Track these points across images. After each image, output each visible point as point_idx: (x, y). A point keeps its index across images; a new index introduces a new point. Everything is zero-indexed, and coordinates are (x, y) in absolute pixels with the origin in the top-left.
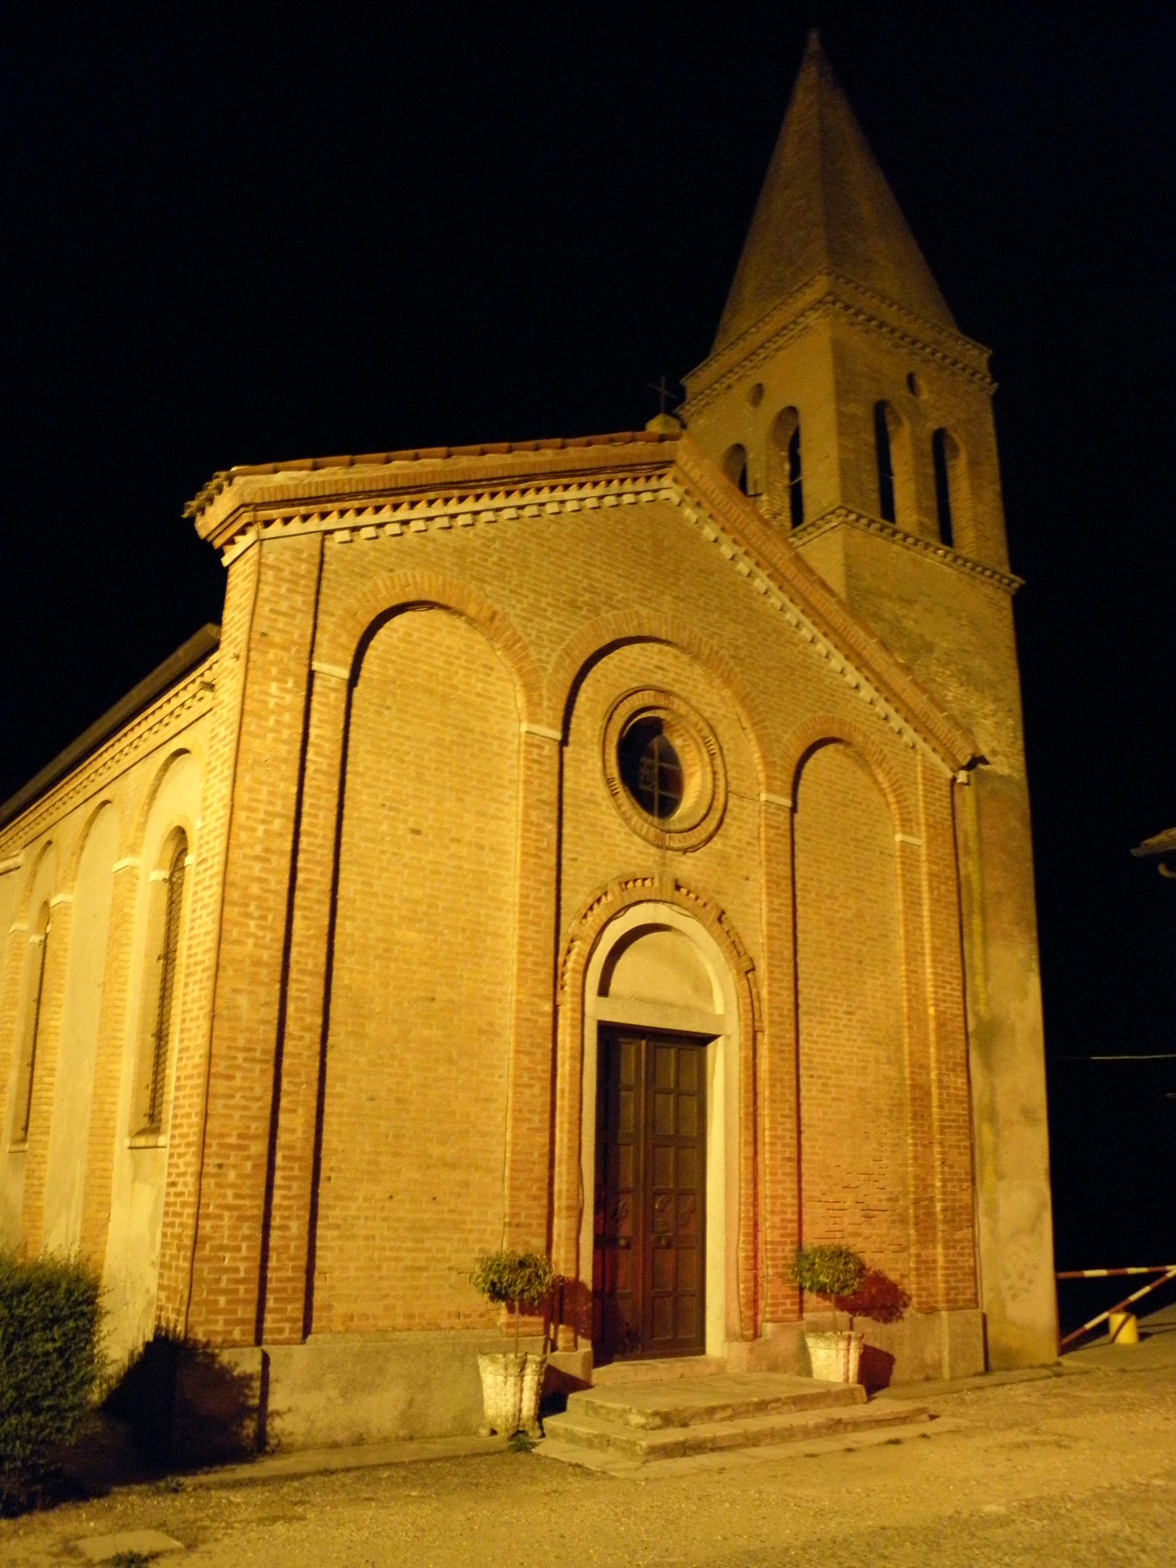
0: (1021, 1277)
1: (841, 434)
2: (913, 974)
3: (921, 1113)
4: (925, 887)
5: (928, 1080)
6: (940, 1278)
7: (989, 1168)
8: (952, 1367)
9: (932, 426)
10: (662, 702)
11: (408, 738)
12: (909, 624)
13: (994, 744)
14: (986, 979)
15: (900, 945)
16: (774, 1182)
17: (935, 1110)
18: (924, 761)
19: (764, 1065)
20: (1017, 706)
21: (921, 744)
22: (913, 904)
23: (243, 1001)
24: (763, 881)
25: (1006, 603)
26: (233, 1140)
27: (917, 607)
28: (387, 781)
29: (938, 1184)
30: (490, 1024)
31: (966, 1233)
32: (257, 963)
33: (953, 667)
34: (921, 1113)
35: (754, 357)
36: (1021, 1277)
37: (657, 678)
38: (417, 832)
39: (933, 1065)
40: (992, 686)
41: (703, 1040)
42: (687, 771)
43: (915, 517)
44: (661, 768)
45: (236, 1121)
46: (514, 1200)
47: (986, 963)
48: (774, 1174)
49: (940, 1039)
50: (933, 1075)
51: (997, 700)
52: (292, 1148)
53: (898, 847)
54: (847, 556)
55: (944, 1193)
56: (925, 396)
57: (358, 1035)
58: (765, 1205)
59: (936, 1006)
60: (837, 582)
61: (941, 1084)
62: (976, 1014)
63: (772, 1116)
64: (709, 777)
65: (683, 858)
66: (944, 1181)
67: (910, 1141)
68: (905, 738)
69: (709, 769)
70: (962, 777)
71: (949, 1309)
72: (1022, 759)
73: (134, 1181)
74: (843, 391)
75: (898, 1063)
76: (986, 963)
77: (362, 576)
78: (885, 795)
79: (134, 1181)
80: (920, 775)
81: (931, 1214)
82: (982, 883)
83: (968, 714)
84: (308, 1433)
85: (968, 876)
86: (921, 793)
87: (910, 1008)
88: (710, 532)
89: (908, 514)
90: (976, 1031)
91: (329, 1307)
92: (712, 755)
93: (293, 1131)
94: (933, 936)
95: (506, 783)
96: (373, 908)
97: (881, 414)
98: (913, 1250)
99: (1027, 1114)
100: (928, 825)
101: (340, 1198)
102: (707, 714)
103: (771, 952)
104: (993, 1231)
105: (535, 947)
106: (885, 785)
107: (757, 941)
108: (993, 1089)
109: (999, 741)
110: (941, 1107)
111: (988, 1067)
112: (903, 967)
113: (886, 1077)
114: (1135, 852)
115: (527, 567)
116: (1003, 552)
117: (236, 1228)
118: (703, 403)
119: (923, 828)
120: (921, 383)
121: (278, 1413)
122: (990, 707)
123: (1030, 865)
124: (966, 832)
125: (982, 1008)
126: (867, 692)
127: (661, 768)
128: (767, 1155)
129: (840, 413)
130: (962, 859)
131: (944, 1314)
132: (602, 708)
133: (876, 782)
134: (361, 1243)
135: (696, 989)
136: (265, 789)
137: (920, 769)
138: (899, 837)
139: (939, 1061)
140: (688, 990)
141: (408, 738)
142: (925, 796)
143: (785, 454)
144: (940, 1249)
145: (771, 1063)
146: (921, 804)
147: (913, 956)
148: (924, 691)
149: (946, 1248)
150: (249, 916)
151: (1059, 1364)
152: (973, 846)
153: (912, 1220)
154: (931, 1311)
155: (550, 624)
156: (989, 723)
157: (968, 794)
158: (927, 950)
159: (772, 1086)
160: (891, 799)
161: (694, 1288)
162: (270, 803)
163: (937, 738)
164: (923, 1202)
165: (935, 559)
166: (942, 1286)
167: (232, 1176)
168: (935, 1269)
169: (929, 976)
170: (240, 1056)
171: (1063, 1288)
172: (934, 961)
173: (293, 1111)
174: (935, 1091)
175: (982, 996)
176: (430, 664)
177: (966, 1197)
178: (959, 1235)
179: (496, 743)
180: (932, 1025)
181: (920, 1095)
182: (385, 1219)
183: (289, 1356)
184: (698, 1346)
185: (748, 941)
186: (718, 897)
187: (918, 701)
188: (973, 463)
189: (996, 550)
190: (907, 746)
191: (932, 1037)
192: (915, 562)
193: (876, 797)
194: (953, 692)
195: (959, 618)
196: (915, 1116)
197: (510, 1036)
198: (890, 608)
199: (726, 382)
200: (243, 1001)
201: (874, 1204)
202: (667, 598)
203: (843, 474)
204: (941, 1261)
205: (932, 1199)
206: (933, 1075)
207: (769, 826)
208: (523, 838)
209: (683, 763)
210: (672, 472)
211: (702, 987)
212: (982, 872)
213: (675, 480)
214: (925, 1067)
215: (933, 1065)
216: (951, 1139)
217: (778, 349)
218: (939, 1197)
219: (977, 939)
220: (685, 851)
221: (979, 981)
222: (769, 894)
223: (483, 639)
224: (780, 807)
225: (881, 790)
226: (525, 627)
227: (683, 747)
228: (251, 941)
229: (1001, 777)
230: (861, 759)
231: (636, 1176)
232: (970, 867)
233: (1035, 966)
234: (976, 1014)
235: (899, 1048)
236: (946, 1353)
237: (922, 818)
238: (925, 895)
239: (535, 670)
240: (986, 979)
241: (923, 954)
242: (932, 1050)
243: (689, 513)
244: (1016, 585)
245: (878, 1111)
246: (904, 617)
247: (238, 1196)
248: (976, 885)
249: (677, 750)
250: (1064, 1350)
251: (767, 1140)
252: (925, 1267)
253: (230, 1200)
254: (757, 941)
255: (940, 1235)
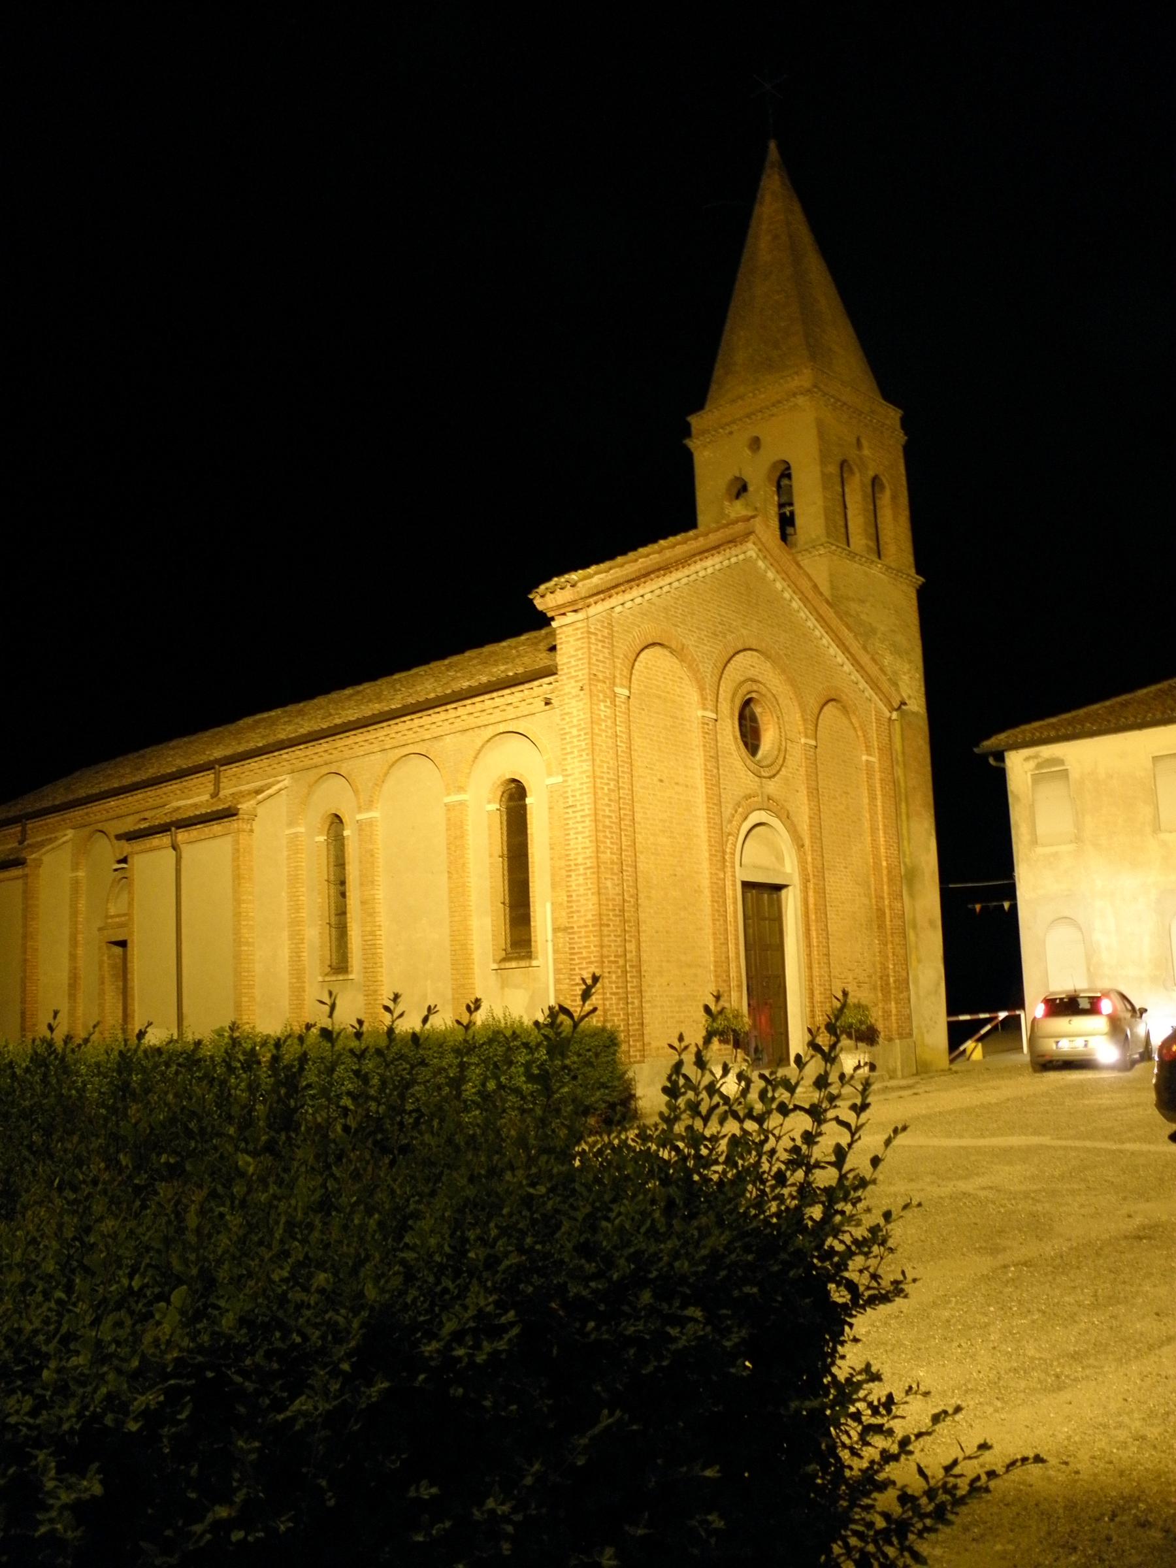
0: (931, 1019)
1: (825, 488)
2: (874, 840)
3: (881, 927)
4: (878, 785)
5: (884, 906)
6: (894, 1021)
7: (914, 957)
8: (902, 1070)
9: (871, 474)
10: (755, 688)
11: (653, 726)
12: (863, 617)
13: (909, 691)
14: (909, 842)
15: (867, 825)
16: (819, 968)
17: (888, 923)
18: (875, 708)
19: (811, 901)
20: (920, 664)
21: (875, 698)
22: (873, 798)
23: (609, 884)
24: (805, 792)
25: (914, 595)
26: (612, 959)
27: (868, 604)
28: (648, 753)
29: (891, 967)
30: (699, 886)
31: (905, 994)
32: (612, 863)
33: (887, 643)
34: (881, 927)
35: (753, 417)
36: (931, 1019)
37: (751, 673)
38: (661, 781)
39: (886, 896)
40: (907, 653)
41: (778, 888)
42: (762, 727)
43: (864, 542)
44: (751, 726)
45: (613, 948)
46: (717, 981)
47: (909, 832)
48: (819, 963)
49: (890, 880)
50: (886, 902)
51: (910, 662)
52: (632, 961)
53: (864, 764)
54: (831, 575)
55: (895, 972)
56: (866, 452)
57: (649, 898)
58: (816, 980)
59: (887, 860)
60: (825, 589)
61: (891, 909)
62: (905, 864)
63: (817, 930)
64: (777, 731)
65: (770, 783)
66: (894, 965)
67: (877, 942)
68: (867, 694)
69: (777, 726)
70: (895, 715)
71: (900, 1039)
72: (924, 700)
73: (502, 988)
74: (824, 457)
75: (869, 896)
76: (909, 832)
77: (627, 631)
78: (856, 731)
79: (502, 988)
80: (874, 717)
81: (888, 984)
82: (906, 782)
83: (895, 673)
84: (651, 1108)
85: (898, 778)
86: (874, 728)
87: (874, 862)
88: (771, 575)
89: (859, 540)
90: (905, 875)
91: (650, 1044)
92: (778, 718)
93: (631, 952)
94: (883, 818)
95: (694, 747)
96: (648, 826)
97: (844, 465)
98: (880, 1005)
99: (931, 923)
100: (879, 749)
101: (649, 986)
102: (774, 692)
103: (812, 834)
104: (917, 994)
105: (715, 842)
106: (857, 725)
107: (804, 827)
108: (914, 909)
109: (912, 689)
110: (891, 921)
111: (912, 896)
112: (870, 838)
113: (864, 905)
114: (976, 750)
115: (694, 614)
116: (911, 559)
117: (618, 1004)
118: (708, 440)
119: (876, 751)
120: (864, 442)
121: (640, 1098)
122: (907, 666)
123: (929, 768)
124: (896, 751)
125: (907, 860)
126: (848, 667)
127: (751, 726)
128: (816, 953)
129: (823, 474)
130: (895, 767)
131: (897, 1041)
132: (729, 696)
133: (852, 723)
134: (659, 1009)
135: (777, 858)
136: (605, 765)
137: (873, 713)
138: (864, 758)
139: (889, 894)
140: (774, 859)
141: (653, 726)
142: (877, 730)
143: (774, 489)
144: (893, 1003)
145: (815, 900)
146: (875, 736)
147: (874, 830)
148: (876, 663)
149: (896, 1003)
150: (606, 837)
151: (950, 1069)
152: (900, 759)
153: (879, 988)
154: (890, 1040)
155: (706, 648)
156: (906, 677)
157: (897, 725)
158: (881, 827)
159: (816, 913)
160: (860, 733)
161: (782, 1030)
162: (608, 773)
163: (883, 693)
164: (884, 977)
165: (876, 570)
166: (895, 1025)
167: (614, 977)
168: (890, 1016)
169: (882, 843)
170: (611, 913)
171: (951, 1025)
172: (885, 833)
173: (631, 941)
174: (887, 911)
175: (908, 853)
176: (657, 680)
177: (904, 974)
178: (901, 996)
179: (688, 723)
180: (885, 872)
181: (881, 913)
182: (667, 996)
183: (641, 1068)
184: (789, 1064)
185: (799, 828)
186: (785, 804)
187: (873, 670)
188: (894, 497)
189: (908, 558)
190: (867, 698)
191: (885, 879)
192: (866, 574)
193: (852, 732)
194: (888, 660)
195: (889, 609)
196: (878, 928)
197: (707, 892)
198: (854, 607)
199: (728, 429)
200: (609, 884)
201: (861, 979)
202: (755, 622)
203: (827, 518)
204: (894, 1011)
205: (888, 976)
206: (886, 902)
207: (807, 758)
208: (706, 779)
209: (760, 722)
210: (752, 537)
211: (780, 858)
212: (905, 776)
213: (754, 544)
214: (882, 898)
215: (886, 896)
216: (897, 940)
217: (773, 415)
218: (892, 974)
219: (904, 817)
220: (770, 778)
221: (905, 843)
222: (809, 800)
223: (677, 661)
224: (811, 746)
225: (855, 728)
226: (696, 651)
227: (761, 713)
228: (609, 851)
229: (913, 713)
230: (845, 710)
231: (756, 970)
232: (899, 772)
233: (933, 833)
234: (905, 864)
235: (869, 887)
236: (899, 1064)
237: (876, 744)
238: (879, 793)
239: (703, 678)
240: (909, 842)
241: (878, 829)
242: (885, 887)
243: (760, 563)
244: (920, 583)
245: (861, 925)
246: (862, 612)
247: (617, 988)
248: (902, 784)
249: (758, 715)
250: (952, 1061)
251: (815, 944)
252: (887, 1015)
253: (615, 990)
254: (804, 827)
255: (892, 996)
